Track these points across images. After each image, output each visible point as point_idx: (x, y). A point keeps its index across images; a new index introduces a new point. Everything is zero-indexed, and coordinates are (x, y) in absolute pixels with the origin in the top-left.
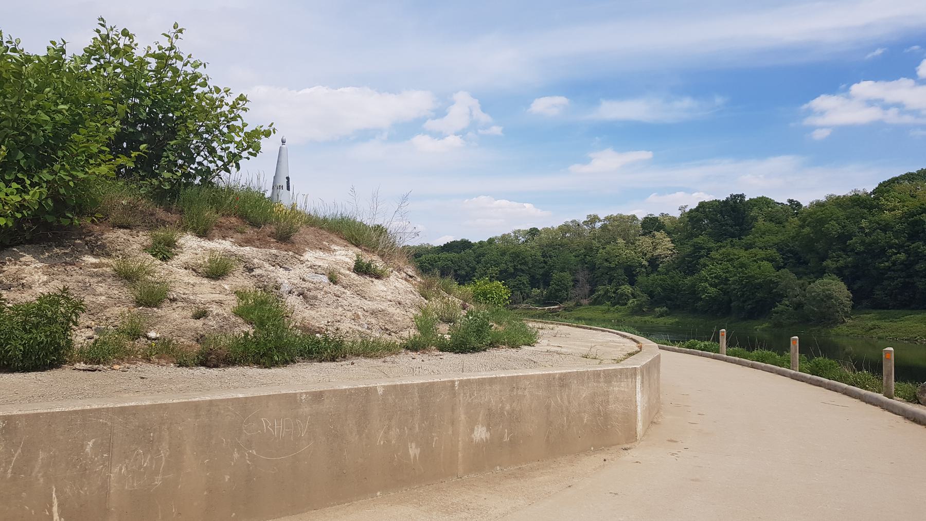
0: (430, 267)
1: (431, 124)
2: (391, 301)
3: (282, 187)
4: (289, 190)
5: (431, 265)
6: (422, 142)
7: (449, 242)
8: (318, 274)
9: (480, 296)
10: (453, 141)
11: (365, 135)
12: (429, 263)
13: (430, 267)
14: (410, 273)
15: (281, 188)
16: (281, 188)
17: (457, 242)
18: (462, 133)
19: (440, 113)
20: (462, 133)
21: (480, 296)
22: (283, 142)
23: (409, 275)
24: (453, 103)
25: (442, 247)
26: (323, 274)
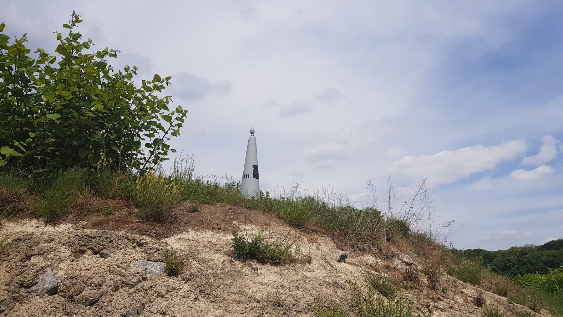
0: (536, 261)
1: (527, 161)
2: (259, 301)
3: (248, 175)
4: (258, 178)
5: (536, 260)
6: (519, 175)
7: (549, 242)
8: (151, 260)
9: (555, 284)
10: (547, 169)
11: (477, 177)
12: (534, 259)
13: (536, 261)
14: (406, 260)
15: (247, 177)
16: (247, 177)
17: (555, 241)
18: (551, 163)
19: (533, 152)
20: (551, 163)
21: (555, 284)
22: (252, 133)
23: (405, 262)
24: (542, 144)
25: (543, 246)
26: (159, 260)
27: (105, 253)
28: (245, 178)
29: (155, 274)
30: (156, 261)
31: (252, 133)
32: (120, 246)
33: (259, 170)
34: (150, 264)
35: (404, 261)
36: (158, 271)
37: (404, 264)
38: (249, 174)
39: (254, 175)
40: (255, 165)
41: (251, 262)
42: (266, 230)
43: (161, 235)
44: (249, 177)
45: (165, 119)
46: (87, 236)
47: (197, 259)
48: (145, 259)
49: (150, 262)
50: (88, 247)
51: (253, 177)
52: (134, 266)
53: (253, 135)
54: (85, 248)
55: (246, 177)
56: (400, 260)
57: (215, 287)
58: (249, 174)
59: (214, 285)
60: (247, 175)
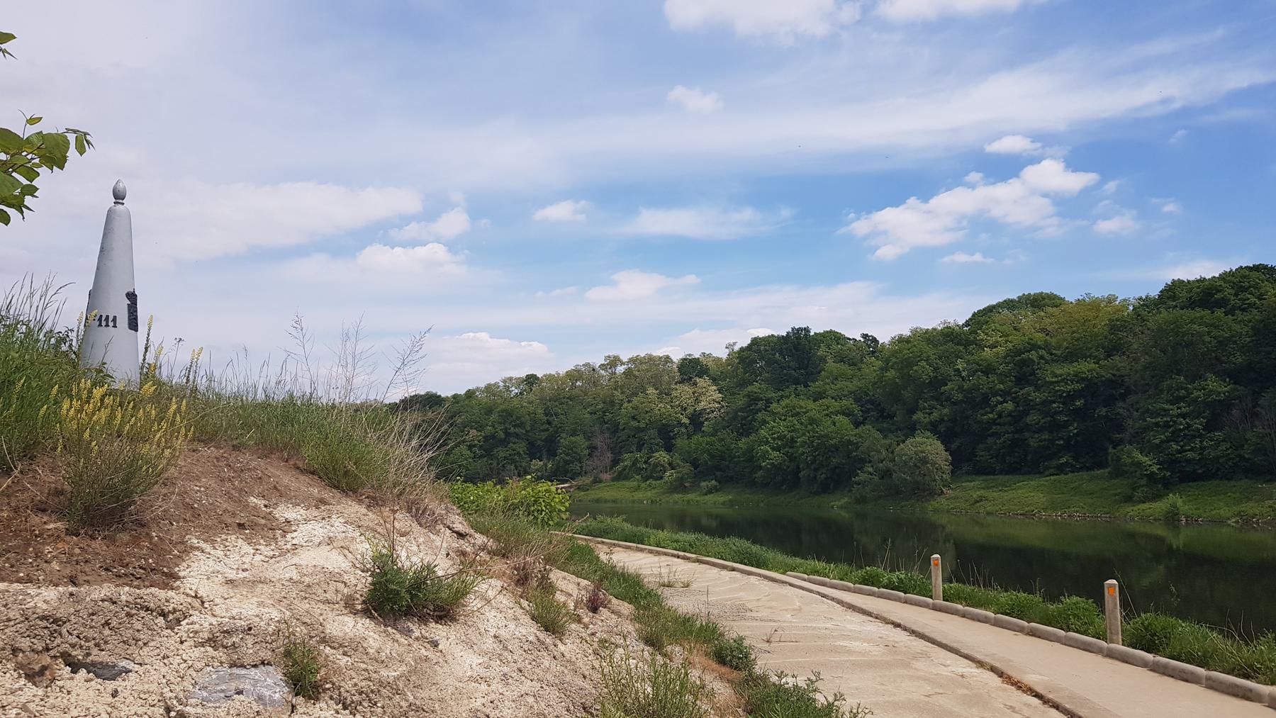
3: (115, 319)
14: (459, 527)
16: (111, 324)
22: (119, 196)
27: (101, 663)
28: (100, 325)
29: (273, 702)
30: (255, 666)
31: (119, 196)
32: (142, 637)
33: (138, 306)
34: (244, 676)
35: (456, 529)
36: (277, 695)
37: (455, 535)
38: (115, 317)
39: (129, 319)
40: (132, 291)
41: (409, 624)
42: (329, 517)
43: (154, 569)
44: (115, 326)
45: (28, 177)
46: (43, 618)
47: (334, 642)
48: (221, 663)
49: (244, 672)
50: (52, 653)
51: (127, 326)
52: (198, 688)
53: (123, 204)
54: (46, 660)
55: (107, 325)
56: (448, 527)
57: (427, 712)
58: (115, 317)
59: (424, 708)
60: (111, 319)
